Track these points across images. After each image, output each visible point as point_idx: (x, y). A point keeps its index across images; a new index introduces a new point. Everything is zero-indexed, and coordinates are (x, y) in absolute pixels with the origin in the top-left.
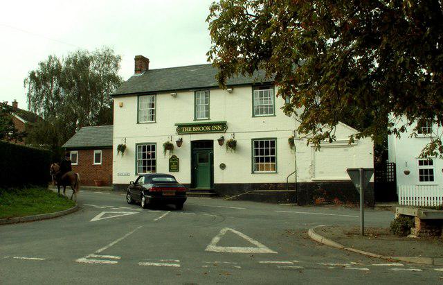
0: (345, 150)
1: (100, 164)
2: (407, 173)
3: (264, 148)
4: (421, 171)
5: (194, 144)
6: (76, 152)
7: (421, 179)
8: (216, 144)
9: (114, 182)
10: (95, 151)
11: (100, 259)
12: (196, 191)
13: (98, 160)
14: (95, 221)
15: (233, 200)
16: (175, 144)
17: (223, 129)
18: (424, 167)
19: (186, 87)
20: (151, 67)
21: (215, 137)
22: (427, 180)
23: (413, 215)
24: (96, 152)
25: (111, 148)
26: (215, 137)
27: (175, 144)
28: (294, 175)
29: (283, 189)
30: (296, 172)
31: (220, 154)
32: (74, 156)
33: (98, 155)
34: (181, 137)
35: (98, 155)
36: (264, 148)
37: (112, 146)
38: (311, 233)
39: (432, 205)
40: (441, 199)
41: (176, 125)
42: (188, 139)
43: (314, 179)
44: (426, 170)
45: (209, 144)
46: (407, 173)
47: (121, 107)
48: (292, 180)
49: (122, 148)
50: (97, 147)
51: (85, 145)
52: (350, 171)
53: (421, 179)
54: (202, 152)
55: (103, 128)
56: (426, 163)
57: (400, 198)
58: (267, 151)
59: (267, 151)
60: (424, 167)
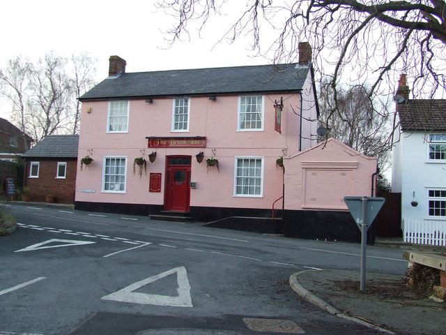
0: (313, 174)
1: (64, 177)
2: (414, 204)
3: (440, 208)
4: (431, 203)
5: (170, 159)
6: (37, 163)
7: (431, 213)
8: (194, 160)
10: (59, 163)
12: (171, 214)
13: (34, 174)
15: (205, 226)
16: (147, 159)
18: (435, 199)
19: (163, 93)
20: (128, 70)
21: (193, 153)
22: (437, 214)
23: (438, 267)
24: (60, 163)
25: (76, 159)
26: (193, 153)
27: (147, 159)
30: (283, 197)
31: (198, 173)
32: (35, 167)
33: (62, 168)
34: (154, 150)
35: (62, 168)
36: (434, 208)
38: (293, 280)
39: (433, 244)
40: (444, 237)
41: (146, 138)
42: (163, 153)
44: (437, 203)
46: (414, 204)
48: (278, 206)
49: (88, 161)
50: (35, 157)
51: (48, 155)
52: (348, 200)
53: (431, 213)
54: (178, 172)
57: (405, 234)
60: (435, 199)
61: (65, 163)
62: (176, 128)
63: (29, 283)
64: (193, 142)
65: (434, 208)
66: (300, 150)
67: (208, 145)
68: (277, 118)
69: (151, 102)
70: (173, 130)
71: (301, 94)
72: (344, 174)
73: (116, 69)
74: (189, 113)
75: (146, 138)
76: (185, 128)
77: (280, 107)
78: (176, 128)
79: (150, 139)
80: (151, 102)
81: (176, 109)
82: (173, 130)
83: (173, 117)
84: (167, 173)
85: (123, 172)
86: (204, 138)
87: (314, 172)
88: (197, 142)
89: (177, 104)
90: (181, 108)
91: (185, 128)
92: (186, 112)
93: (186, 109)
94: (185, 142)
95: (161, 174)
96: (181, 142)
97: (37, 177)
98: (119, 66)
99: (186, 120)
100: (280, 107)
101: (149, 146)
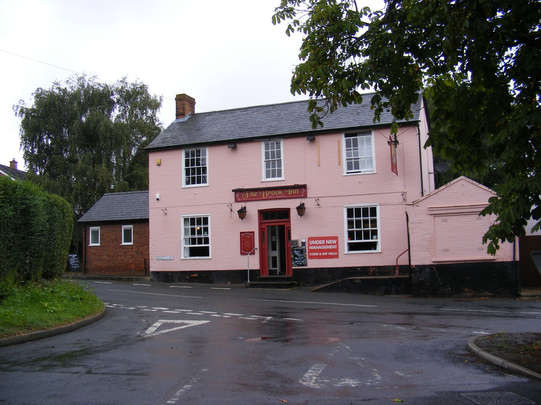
0: (443, 221)
1: (131, 243)
5: (264, 214)
6: (98, 228)
8: (294, 213)
9: (151, 269)
11: (514, 313)
13: (128, 239)
14: (207, 320)
17: (300, 193)
21: (292, 204)
24: (124, 227)
28: (407, 252)
29: (374, 274)
30: (409, 250)
34: (243, 205)
35: (128, 232)
37: (148, 219)
43: (434, 259)
45: (285, 213)
47: (159, 165)
48: (403, 261)
55: (134, 196)
56: (200, 242)
58: (358, 226)
59: (358, 226)
61: (132, 226)
62: (268, 176)
63: (170, 330)
64: (290, 192)
65: (354, 219)
66: (423, 196)
67: (309, 194)
68: (393, 157)
69: (234, 148)
70: (264, 179)
71: (418, 126)
72: (446, 221)
73: (184, 109)
74: (282, 158)
75: (233, 191)
76: (280, 175)
77: (394, 143)
78: (268, 176)
79: (236, 191)
80: (234, 148)
81: (267, 154)
82: (264, 179)
83: (264, 165)
84: (261, 230)
85: (186, 230)
86: (304, 187)
87: (445, 218)
88: (296, 191)
89: (267, 148)
90: (273, 153)
91: (280, 175)
92: (279, 156)
93: (279, 153)
94: (280, 192)
95: (253, 232)
96: (275, 193)
97: (99, 244)
98: (187, 107)
99: (280, 165)
100: (394, 143)
101: (236, 201)
